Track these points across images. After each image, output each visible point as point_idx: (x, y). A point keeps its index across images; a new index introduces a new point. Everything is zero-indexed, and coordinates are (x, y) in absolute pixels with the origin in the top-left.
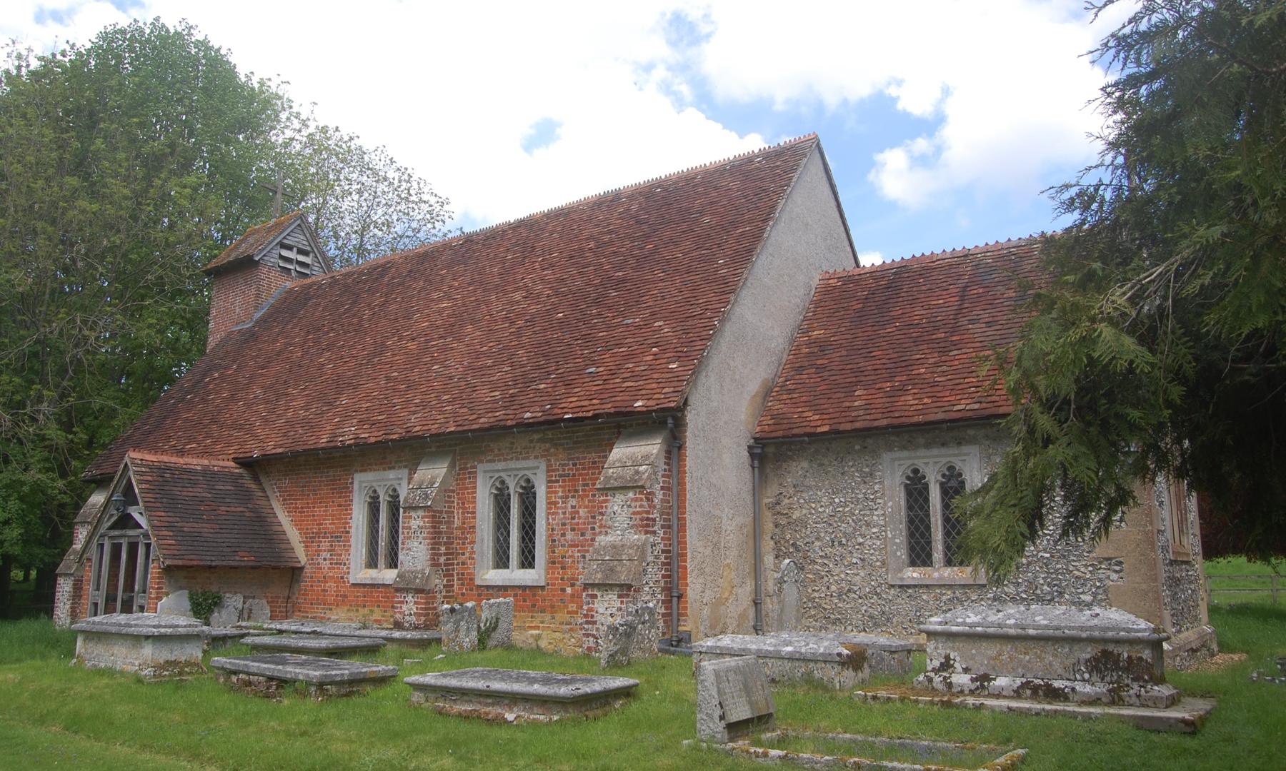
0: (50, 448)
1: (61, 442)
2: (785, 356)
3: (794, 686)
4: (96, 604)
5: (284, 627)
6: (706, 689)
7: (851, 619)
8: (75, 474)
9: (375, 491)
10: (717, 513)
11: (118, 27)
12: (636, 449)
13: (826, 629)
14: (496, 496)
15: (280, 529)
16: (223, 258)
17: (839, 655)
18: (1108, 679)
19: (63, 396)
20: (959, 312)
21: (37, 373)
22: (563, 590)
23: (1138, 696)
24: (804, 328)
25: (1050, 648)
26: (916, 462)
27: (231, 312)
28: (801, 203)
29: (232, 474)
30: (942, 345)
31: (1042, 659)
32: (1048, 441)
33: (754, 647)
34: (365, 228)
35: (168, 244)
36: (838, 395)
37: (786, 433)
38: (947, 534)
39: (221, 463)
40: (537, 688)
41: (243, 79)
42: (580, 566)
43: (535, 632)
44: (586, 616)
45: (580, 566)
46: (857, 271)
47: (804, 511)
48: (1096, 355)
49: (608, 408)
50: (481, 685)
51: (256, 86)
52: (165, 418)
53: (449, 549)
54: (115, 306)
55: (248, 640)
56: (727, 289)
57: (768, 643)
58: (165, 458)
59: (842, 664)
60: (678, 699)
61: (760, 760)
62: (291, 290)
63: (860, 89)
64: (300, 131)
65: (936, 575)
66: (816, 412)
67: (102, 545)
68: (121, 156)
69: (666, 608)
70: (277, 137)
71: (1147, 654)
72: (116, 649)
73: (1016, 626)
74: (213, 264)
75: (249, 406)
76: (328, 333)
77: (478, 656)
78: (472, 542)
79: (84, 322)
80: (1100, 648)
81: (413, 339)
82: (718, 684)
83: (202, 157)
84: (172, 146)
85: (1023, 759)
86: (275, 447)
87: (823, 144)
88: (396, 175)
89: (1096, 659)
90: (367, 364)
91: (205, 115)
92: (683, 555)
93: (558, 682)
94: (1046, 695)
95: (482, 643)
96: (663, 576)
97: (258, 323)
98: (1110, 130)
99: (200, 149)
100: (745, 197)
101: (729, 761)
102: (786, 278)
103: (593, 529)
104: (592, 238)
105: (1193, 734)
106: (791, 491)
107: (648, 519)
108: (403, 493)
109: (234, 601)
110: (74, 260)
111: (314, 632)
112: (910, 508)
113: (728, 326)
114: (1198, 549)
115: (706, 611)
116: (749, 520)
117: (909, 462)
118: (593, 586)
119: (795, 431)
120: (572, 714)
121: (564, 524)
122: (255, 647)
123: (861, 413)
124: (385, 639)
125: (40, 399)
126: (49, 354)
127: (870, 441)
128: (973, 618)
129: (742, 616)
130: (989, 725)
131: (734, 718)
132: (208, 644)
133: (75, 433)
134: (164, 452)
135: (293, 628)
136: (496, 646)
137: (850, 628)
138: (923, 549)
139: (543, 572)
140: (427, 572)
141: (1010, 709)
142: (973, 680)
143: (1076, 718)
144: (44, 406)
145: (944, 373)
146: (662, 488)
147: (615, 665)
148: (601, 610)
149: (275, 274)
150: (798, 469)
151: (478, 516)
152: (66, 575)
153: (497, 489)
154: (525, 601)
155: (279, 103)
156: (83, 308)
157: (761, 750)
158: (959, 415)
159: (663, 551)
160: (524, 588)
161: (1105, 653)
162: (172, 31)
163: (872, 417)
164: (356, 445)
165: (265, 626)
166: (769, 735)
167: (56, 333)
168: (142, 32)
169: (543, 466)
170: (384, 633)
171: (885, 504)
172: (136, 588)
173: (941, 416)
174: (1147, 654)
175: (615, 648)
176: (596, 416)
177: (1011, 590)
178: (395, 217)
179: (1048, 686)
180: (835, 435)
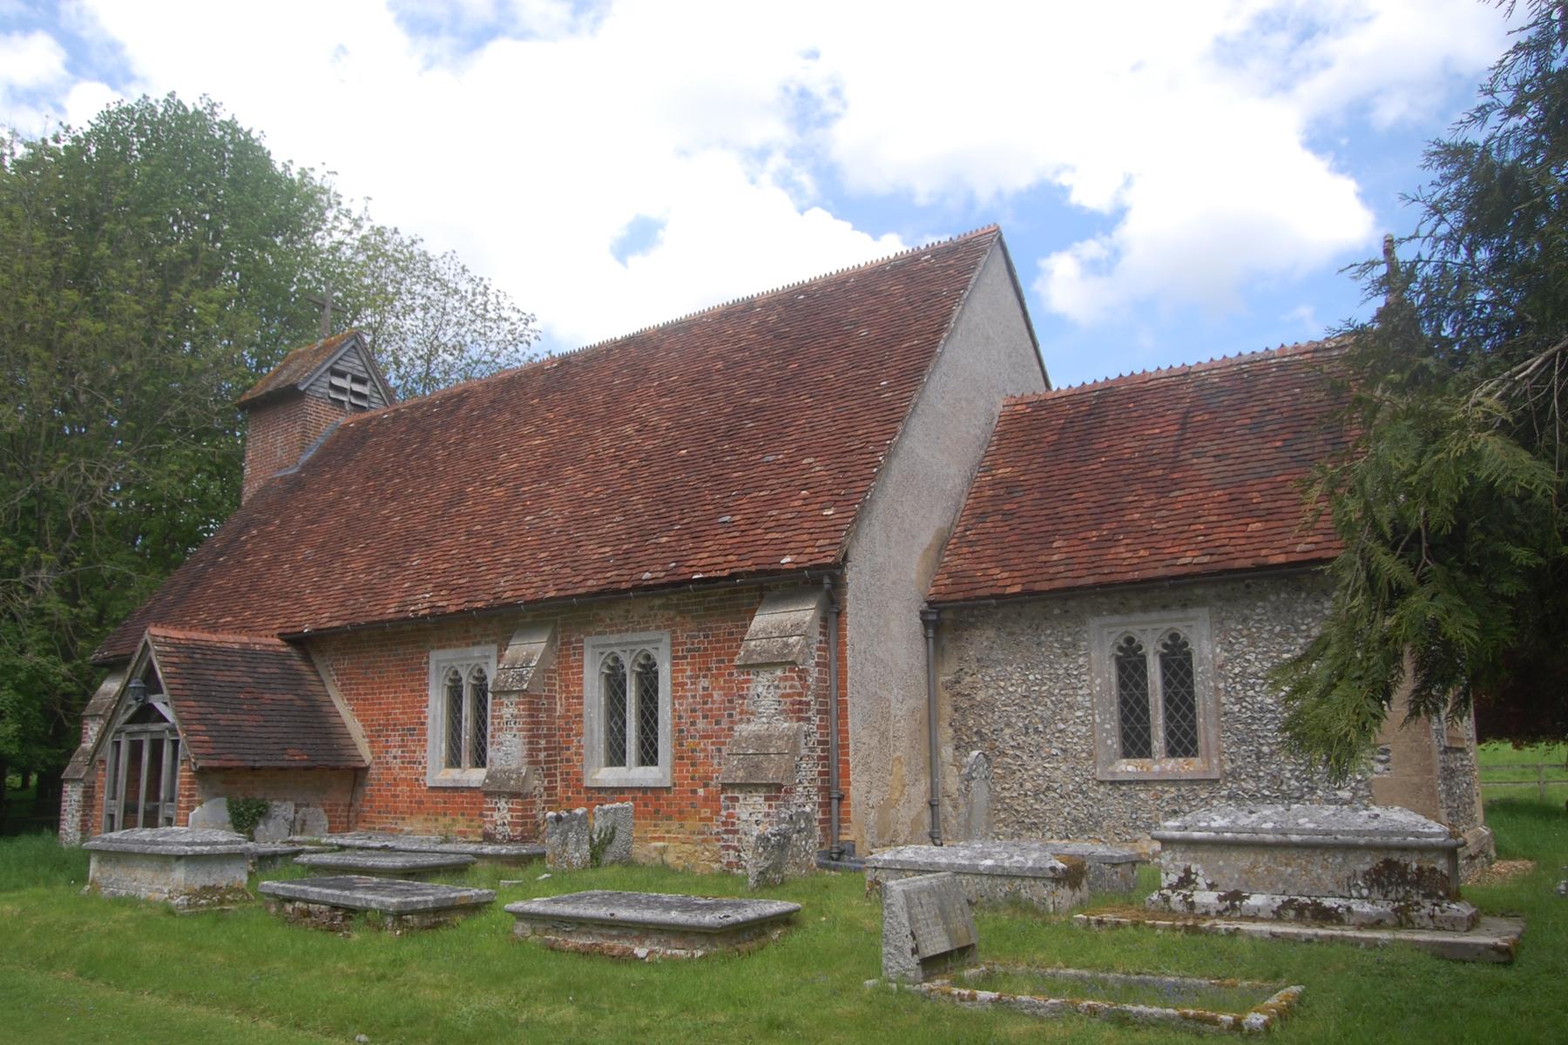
0: (50, 625)
1: (65, 617)
2: (963, 500)
3: (995, 909)
4: (112, 816)
5: (347, 841)
6: (894, 915)
7: (1050, 823)
8: (82, 657)
9: (456, 673)
10: (884, 694)
11: (124, 105)
12: (784, 617)
13: (1019, 836)
14: (608, 676)
15: (337, 720)
16: (260, 389)
17: (1053, 869)
18: (1392, 895)
19: (65, 561)
20: (1180, 443)
21: (32, 533)
22: (694, 792)
23: (1432, 917)
24: (987, 464)
25: (1318, 858)
26: (1130, 628)
27: (269, 455)
28: (980, 311)
29: (278, 654)
30: (1160, 484)
31: (1308, 872)
32: (1398, 593)
33: (944, 860)
34: (433, 352)
35: (190, 373)
36: (1031, 547)
37: (968, 595)
38: (1169, 718)
39: (264, 640)
40: (675, 916)
41: (280, 169)
42: (715, 761)
43: (660, 844)
44: (724, 823)
45: (715, 761)
46: (1049, 395)
47: (991, 691)
48: (1482, 474)
49: (748, 565)
50: (602, 912)
51: (296, 177)
52: (192, 586)
53: (550, 744)
54: (127, 449)
55: (304, 859)
56: (893, 418)
57: (959, 854)
58: (195, 635)
59: (1057, 880)
60: (851, 926)
61: (967, 1004)
62: (345, 427)
63: (1021, 179)
64: (350, 233)
65: (1156, 768)
66: (1004, 568)
67: (118, 744)
68: (130, 264)
69: (824, 813)
70: (323, 240)
71: (1441, 865)
72: (139, 873)
73: (1274, 830)
74: (248, 396)
75: (296, 570)
76: (392, 478)
77: (591, 875)
78: (579, 734)
79: (90, 470)
80: (1382, 857)
81: (500, 484)
82: (910, 908)
83: (231, 266)
84: (194, 251)
85: (1300, 999)
86: (331, 619)
87: (1006, 238)
88: (470, 287)
89: (1377, 871)
90: (442, 516)
91: (233, 213)
92: (844, 747)
93: (701, 907)
94: (1314, 917)
95: (596, 857)
96: (820, 773)
97: (305, 468)
98: (1435, 188)
99: (228, 256)
100: (911, 304)
101: (927, 1006)
102: (964, 404)
103: (731, 715)
104: (720, 357)
105: (1508, 964)
106: (974, 666)
107: (800, 703)
108: (491, 675)
109: (284, 810)
110: (75, 394)
111: (385, 848)
112: (1123, 685)
113: (895, 463)
114: (1472, 734)
115: (873, 816)
116: (923, 702)
117: (1122, 630)
118: (733, 786)
119: (979, 593)
120: (720, 948)
121: (694, 711)
122: (314, 868)
123: (1062, 568)
124: (474, 855)
125: (37, 565)
126: (47, 510)
127: (1072, 603)
128: (1219, 822)
129: (916, 822)
130: (1249, 956)
131: (929, 951)
132: (254, 865)
133: (81, 607)
134: (192, 628)
135: (358, 843)
136: (613, 862)
137: (1049, 834)
138: (1139, 736)
139: (668, 770)
140: (524, 771)
141: (1273, 935)
142: (1220, 899)
143: (1358, 945)
144: (42, 573)
145: (1163, 520)
146: (818, 664)
147: (767, 884)
148: (744, 817)
149: (324, 407)
150: (981, 641)
151: (586, 701)
152: (74, 780)
153: (609, 667)
154: (646, 805)
155: (324, 198)
156: (88, 453)
157: (966, 992)
158: (1185, 570)
159: (820, 743)
160: (644, 790)
161: (1389, 864)
162: (191, 110)
163: (1075, 574)
164: (432, 615)
165: (324, 840)
166: (973, 971)
167: (55, 483)
168: (154, 112)
169: (667, 639)
170: (472, 848)
171: (1092, 681)
172: (162, 795)
173: (1161, 572)
174: (1441, 865)
175: (766, 864)
176: (733, 576)
177: (1250, 785)
178: (468, 339)
179: (1317, 905)
180: (1029, 596)
